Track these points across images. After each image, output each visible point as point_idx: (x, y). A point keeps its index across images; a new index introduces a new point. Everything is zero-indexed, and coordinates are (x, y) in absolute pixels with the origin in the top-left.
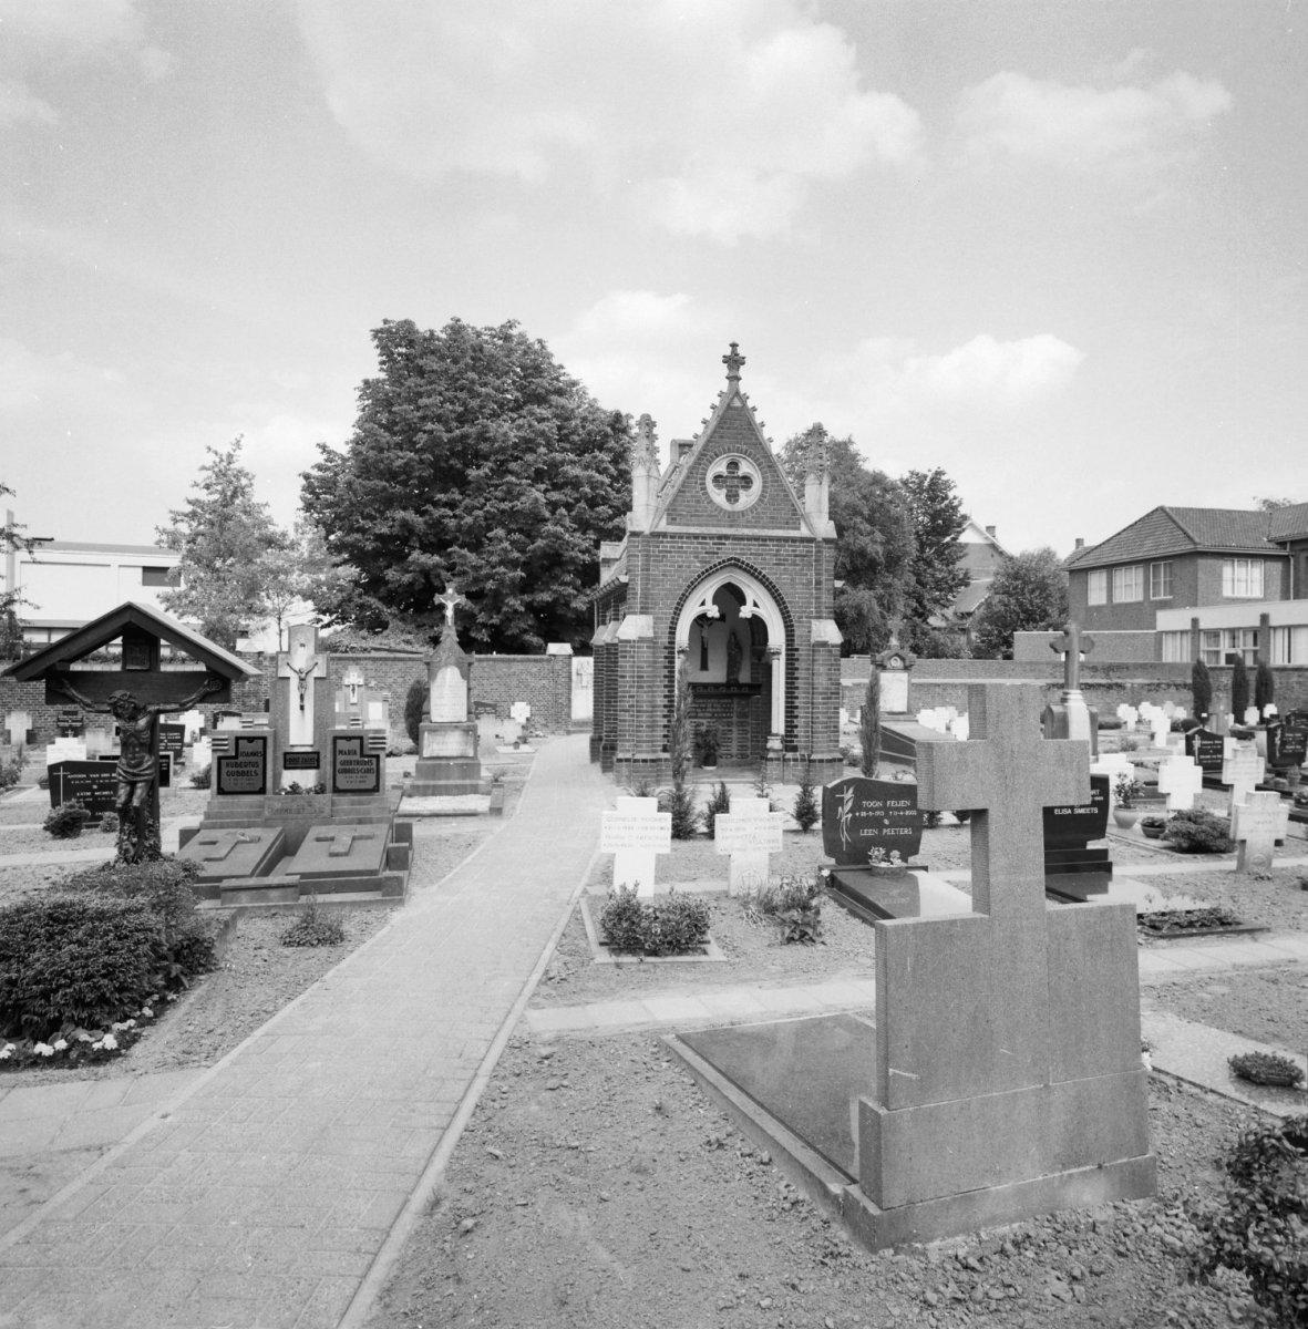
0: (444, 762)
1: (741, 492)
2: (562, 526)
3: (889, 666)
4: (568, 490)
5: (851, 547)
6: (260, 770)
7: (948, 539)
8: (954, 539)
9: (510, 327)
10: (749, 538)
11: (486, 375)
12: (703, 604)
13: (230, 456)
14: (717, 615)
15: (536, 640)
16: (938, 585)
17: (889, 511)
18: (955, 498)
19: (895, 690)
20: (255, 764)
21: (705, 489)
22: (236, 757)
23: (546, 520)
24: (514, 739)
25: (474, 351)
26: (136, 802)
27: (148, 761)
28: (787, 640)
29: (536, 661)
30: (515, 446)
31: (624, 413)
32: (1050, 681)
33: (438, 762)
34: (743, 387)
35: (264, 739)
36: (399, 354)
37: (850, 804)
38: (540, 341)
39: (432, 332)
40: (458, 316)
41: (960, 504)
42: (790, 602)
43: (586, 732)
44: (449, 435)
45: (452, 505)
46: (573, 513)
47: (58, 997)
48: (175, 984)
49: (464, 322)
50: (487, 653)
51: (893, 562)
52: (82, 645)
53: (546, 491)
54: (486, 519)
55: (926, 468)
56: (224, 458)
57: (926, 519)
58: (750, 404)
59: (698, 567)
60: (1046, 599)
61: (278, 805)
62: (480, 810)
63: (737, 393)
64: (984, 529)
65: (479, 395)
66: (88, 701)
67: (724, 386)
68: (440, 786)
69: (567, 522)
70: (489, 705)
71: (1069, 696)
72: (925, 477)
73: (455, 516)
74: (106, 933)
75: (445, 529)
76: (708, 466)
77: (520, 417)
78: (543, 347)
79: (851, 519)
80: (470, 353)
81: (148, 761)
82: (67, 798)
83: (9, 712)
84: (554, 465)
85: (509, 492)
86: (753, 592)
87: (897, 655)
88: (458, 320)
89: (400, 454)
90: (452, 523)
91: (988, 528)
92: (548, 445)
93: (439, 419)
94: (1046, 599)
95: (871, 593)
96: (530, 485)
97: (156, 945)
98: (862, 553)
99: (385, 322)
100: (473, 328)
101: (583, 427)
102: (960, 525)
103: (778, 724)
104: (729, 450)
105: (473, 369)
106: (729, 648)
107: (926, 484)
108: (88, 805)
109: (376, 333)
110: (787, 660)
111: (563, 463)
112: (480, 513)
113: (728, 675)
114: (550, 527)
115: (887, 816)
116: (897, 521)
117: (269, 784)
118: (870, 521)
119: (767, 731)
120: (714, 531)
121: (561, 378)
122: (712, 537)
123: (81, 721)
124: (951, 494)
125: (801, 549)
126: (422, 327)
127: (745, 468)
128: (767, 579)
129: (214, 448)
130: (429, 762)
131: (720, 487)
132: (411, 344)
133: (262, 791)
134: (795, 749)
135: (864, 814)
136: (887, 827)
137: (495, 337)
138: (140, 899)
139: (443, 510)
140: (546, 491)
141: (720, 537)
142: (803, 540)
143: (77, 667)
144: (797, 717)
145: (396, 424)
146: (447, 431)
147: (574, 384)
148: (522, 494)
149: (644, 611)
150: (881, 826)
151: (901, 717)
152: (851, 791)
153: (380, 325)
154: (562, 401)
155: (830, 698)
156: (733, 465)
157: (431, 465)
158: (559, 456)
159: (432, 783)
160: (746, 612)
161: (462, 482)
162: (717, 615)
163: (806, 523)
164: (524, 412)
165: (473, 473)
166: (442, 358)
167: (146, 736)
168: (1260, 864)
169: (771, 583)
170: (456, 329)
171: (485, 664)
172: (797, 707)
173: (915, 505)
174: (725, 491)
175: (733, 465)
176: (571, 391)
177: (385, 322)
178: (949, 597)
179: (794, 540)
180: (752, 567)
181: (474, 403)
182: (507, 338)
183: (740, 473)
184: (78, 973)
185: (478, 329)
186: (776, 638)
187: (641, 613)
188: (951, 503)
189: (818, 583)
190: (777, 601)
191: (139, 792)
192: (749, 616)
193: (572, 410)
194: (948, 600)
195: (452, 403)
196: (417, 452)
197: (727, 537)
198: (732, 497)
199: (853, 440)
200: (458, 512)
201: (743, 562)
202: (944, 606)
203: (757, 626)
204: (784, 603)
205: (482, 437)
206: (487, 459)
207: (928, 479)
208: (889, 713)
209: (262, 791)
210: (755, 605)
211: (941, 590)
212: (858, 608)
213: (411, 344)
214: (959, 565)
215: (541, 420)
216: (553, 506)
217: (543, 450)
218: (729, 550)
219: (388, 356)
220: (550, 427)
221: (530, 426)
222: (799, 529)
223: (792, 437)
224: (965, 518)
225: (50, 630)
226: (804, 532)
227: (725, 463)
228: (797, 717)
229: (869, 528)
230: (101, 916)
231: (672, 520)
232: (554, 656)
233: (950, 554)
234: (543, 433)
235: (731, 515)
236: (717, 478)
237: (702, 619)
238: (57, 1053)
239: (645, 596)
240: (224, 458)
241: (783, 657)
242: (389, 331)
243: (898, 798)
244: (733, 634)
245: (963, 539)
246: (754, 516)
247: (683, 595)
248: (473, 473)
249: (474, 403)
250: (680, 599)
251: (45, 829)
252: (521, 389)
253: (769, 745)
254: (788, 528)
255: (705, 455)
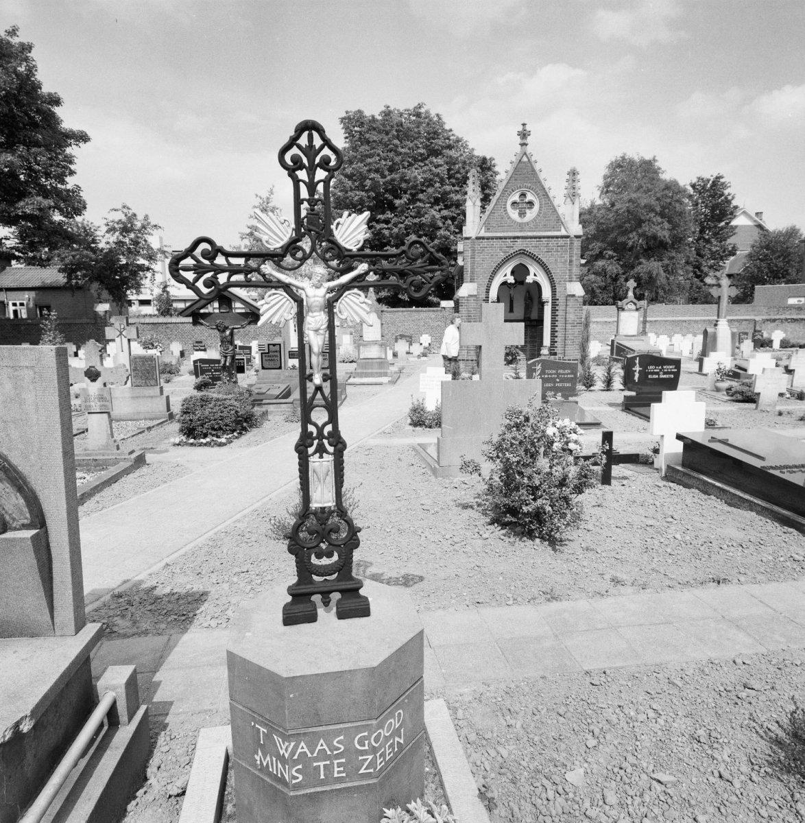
0: (370, 361)
1: (527, 211)
2: (449, 231)
3: (626, 308)
4: (453, 209)
5: (647, 233)
6: (279, 359)
7: (723, 224)
8: (727, 224)
9: (420, 108)
10: (531, 238)
11: (405, 140)
12: (505, 275)
13: (268, 198)
14: (513, 281)
15: (435, 300)
16: (714, 256)
17: (675, 208)
18: (729, 195)
19: (629, 320)
20: (276, 356)
21: (505, 208)
22: (268, 353)
23: (440, 228)
24: (418, 353)
25: (398, 126)
26: (228, 364)
27: (231, 348)
28: (552, 294)
29: (433, 311)
30: (422, 184)
31: (488, 157)
32: (764, 317)
33: (368, 361)
34: (529, 149)
35: (280, 345)
36: (356, 132)
37: (539, 371)
38: (438, 115)
39: (373, 117)
40: (389, 104)
41: (733, 198)
42: (554, 273)
43: (229, 292)
44: (384, 180)
45: (387, 222)
46: (456, 223)
47: (206, 426)
48: (245, 429)
49: (392, 108)
50: (410, 307)
51: (678, 241)
52: (84, 735)
53: (440, 211)
54: (406, 229)
55: (709, 174)
56: (265, 200)
57: (707, 211)
58: (533, 159)
59: (502, 256)
60: (788, 262)
61: (287, 374)
62: (384, 382)
63: (525, 154)
64: (754, 215)
65: (401, 153)
66: (208, 324)
67: (518, 149)
68: (369, 373)
69: (452, 228)
70: (408, 336)
71: (719, 323)
72: (708, 180)
73: (388, 228)
74: (220, 405)
75: (384, 236)
76: (508, 197)
77: (426, 165)
78: (440, 119)
79: (648, 214)
80: (396, 128)
81: (231, 348)
82: (202, 374)
83: (171, 341)
84: (446, 193)
85: (419, 212)
86: (533, 269)
87: (632, 302)
88: (388, 107)
89: (358, 193)
90: (386, 232)
91: (757, 214)
92: (442, 182)
93: (377, 171)
94: (788, 262)
95: (660, 263)
96: (431, 207)
97: (237, 412)
98: (655, 237)
99: (347, 112)
100: (398, 111)
101: (464, 168)
102: (732, 213)
103: (547, 341)
104: (520, 188)
105: (398, 137)
106: (525, 300)
107: (709, 186)
108: (210, 378)
109: (342, 120)
110: (552, 305)
111: (449, 193)
112: (402, 226)
113: (525, 313)
114: (442, 232)
115: (558, 377)
116: (681, 214)
117: (283, 365)
118: (662, 215)
119: (541, 344)
120: (511, 234)
121: (452, 138)
122: (510, 238)
123: (204, 346)
124: (726, 192)
125: (561, 242)
126: (368, 113)
127: (529, 197)
128: (541, 261)
129: (259, 195)
130: (364, 361)
131: (515, 209)
132: (362, 125)
133: (280, 368)
134: (555, 354)
135: (546, 376)
136: (558, 382)
137: (411, 115)
138: (230, 396)
139: (381, 225)
140: (440, 210)
141: (514, 238)
142: (562, 237)
143: (202, 311)
144: (556, 337)
145: (355, 175)
146: (382, 178)
147: (458, 141)
148: (426, 213)
149: (472, 281)
150: (555, 382)
151: (633, 338)
152: (540, 365)
153: (344, 115)
154: (452, 153)
155: (576, 326)
156: (523, 195)
157: (374, 198)
158: (448, 188)
159: (365, 371)
160: (529, 279)
161: (392, 208)
162: (513, 281)
163: (565, 228)
164: (427, 162)
165: (397, 202)
166: (380, 132)
167: (229, 338)
168: (769, 405)
169: (543, 263)
170: (387, 113)
171: (405, 313)
172: (557, 331)
173: (700, 201)
174: (518, 211)
175: (523, 195)
176: (457, 146)
177: (347, 112)
178: (720, 264)
179: (557, 237)
180: (532, 254)
181: (398, 159)
182: (418, 115)
183: (527, 200)
184: (212, 418)
185: (401, 111)
186: (546, 294)
187: (470, 282)
188: (726, 198)
189: (571, 261)
190: (547, 273)
191: (228, 360)
192: (531, 281)
193: (457, 158)
194: (719, 266)
195: (385, 160)
196: (367, 191)
197: (518, 238)
198: (522, 214)
199: (656, 158)
200: (390, 226)
201: (527, 251)
202: (716, 270)
203: (537, 286)
204: (551, 273)
205: (403, 179)
206: (405, 193)
207: (711, 182)
208: (626, 336)
209: (280, 368)
210: (535, 275)
211: (715, 259)
212: (650, 273)
213: (362, 125)
214: (729, 241)
215: (437, 166)
216: (445, 218)
217: (438, 185)
218: (519, 245)
219: (349, 134)
220: (443, 171)
221: (431, 170)
222: (560, 231)
223: (613, 159)
224: (736, 207)
225: (185, 301)
226: (563, 232)
227: (518, 195)
228: (556, 337)
229: (660, 220)
230: (218, 400)
231: (488, 230)
232: (444, 308)
233: (720, 236)
234: (438, 175)
235: (520, 225)
236: (514, 203)
237: (504, 283)
238: (207, 442)
239: (472, 273)
240: (265, 200)
241: (550, 304)
242: (349, 118)
243: (564, 369)
244: (528, 292)
245: (734, 223)
246: (535, 224)
247: (494, 271)
248: (397, 202)
249: (398, 159)
250: (492, 273)
251: (194, 389)
252: (426, 147)
253: (541, 352)
254: (554, 231)
255: (507, 191)
